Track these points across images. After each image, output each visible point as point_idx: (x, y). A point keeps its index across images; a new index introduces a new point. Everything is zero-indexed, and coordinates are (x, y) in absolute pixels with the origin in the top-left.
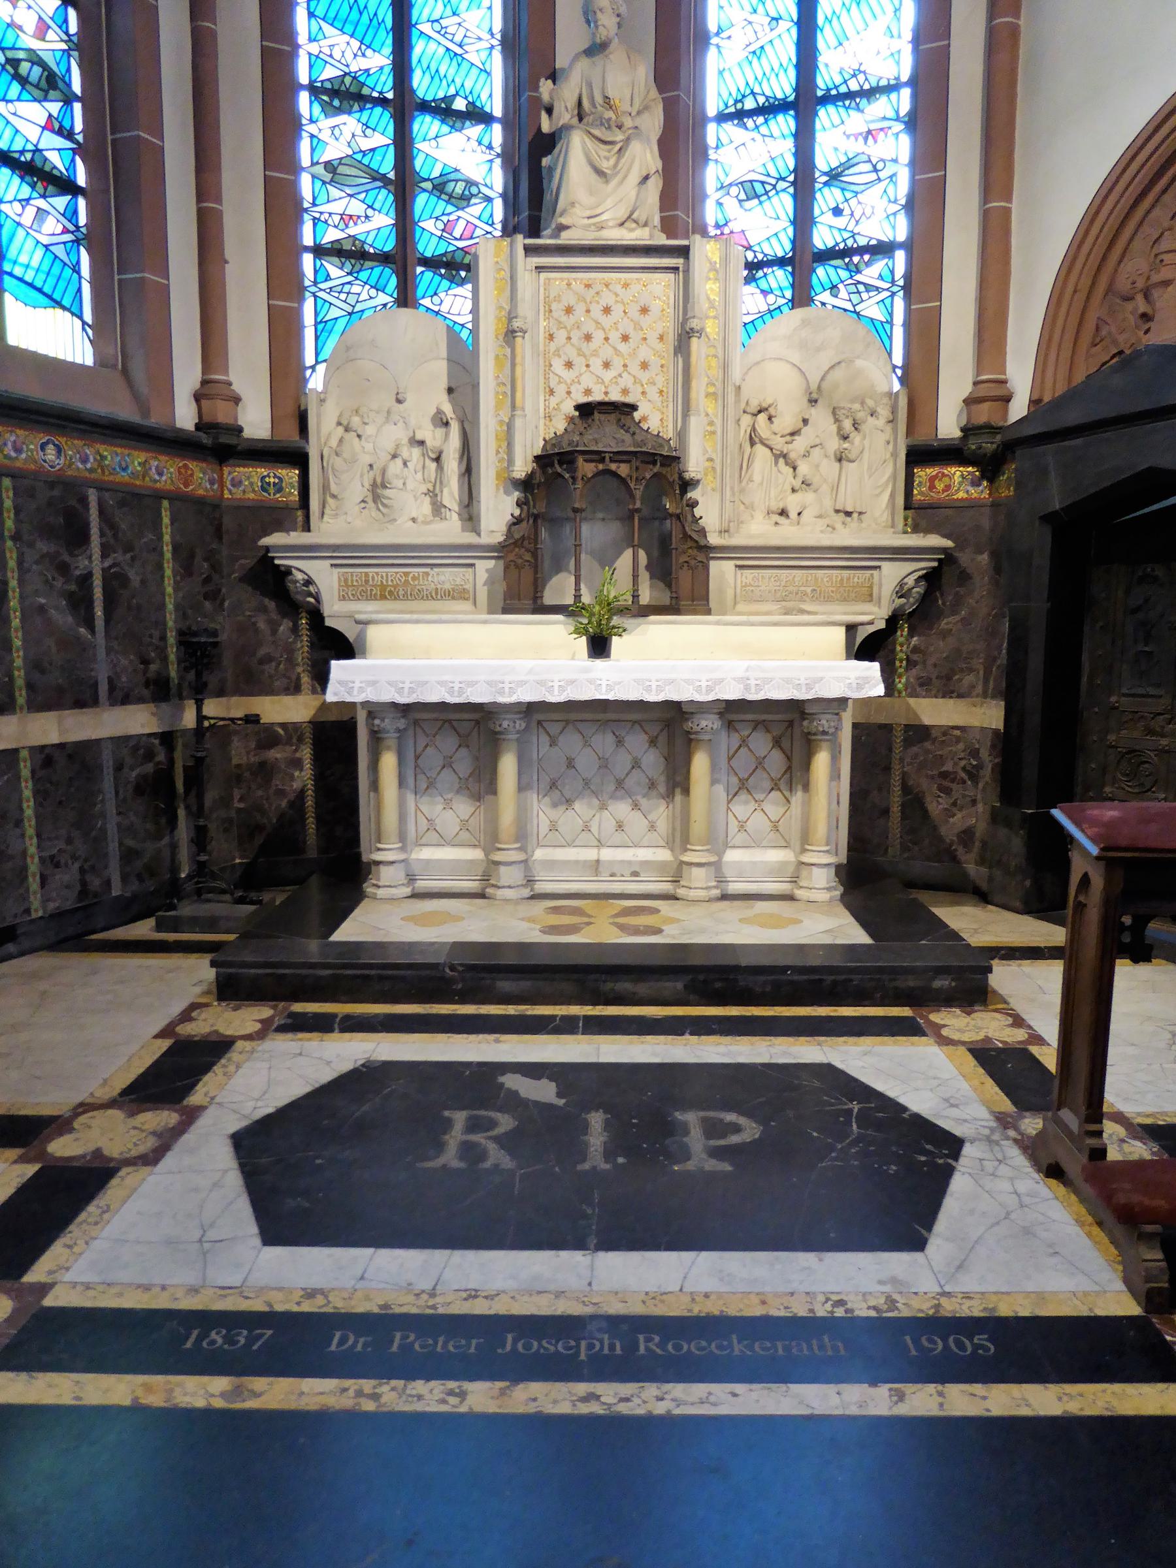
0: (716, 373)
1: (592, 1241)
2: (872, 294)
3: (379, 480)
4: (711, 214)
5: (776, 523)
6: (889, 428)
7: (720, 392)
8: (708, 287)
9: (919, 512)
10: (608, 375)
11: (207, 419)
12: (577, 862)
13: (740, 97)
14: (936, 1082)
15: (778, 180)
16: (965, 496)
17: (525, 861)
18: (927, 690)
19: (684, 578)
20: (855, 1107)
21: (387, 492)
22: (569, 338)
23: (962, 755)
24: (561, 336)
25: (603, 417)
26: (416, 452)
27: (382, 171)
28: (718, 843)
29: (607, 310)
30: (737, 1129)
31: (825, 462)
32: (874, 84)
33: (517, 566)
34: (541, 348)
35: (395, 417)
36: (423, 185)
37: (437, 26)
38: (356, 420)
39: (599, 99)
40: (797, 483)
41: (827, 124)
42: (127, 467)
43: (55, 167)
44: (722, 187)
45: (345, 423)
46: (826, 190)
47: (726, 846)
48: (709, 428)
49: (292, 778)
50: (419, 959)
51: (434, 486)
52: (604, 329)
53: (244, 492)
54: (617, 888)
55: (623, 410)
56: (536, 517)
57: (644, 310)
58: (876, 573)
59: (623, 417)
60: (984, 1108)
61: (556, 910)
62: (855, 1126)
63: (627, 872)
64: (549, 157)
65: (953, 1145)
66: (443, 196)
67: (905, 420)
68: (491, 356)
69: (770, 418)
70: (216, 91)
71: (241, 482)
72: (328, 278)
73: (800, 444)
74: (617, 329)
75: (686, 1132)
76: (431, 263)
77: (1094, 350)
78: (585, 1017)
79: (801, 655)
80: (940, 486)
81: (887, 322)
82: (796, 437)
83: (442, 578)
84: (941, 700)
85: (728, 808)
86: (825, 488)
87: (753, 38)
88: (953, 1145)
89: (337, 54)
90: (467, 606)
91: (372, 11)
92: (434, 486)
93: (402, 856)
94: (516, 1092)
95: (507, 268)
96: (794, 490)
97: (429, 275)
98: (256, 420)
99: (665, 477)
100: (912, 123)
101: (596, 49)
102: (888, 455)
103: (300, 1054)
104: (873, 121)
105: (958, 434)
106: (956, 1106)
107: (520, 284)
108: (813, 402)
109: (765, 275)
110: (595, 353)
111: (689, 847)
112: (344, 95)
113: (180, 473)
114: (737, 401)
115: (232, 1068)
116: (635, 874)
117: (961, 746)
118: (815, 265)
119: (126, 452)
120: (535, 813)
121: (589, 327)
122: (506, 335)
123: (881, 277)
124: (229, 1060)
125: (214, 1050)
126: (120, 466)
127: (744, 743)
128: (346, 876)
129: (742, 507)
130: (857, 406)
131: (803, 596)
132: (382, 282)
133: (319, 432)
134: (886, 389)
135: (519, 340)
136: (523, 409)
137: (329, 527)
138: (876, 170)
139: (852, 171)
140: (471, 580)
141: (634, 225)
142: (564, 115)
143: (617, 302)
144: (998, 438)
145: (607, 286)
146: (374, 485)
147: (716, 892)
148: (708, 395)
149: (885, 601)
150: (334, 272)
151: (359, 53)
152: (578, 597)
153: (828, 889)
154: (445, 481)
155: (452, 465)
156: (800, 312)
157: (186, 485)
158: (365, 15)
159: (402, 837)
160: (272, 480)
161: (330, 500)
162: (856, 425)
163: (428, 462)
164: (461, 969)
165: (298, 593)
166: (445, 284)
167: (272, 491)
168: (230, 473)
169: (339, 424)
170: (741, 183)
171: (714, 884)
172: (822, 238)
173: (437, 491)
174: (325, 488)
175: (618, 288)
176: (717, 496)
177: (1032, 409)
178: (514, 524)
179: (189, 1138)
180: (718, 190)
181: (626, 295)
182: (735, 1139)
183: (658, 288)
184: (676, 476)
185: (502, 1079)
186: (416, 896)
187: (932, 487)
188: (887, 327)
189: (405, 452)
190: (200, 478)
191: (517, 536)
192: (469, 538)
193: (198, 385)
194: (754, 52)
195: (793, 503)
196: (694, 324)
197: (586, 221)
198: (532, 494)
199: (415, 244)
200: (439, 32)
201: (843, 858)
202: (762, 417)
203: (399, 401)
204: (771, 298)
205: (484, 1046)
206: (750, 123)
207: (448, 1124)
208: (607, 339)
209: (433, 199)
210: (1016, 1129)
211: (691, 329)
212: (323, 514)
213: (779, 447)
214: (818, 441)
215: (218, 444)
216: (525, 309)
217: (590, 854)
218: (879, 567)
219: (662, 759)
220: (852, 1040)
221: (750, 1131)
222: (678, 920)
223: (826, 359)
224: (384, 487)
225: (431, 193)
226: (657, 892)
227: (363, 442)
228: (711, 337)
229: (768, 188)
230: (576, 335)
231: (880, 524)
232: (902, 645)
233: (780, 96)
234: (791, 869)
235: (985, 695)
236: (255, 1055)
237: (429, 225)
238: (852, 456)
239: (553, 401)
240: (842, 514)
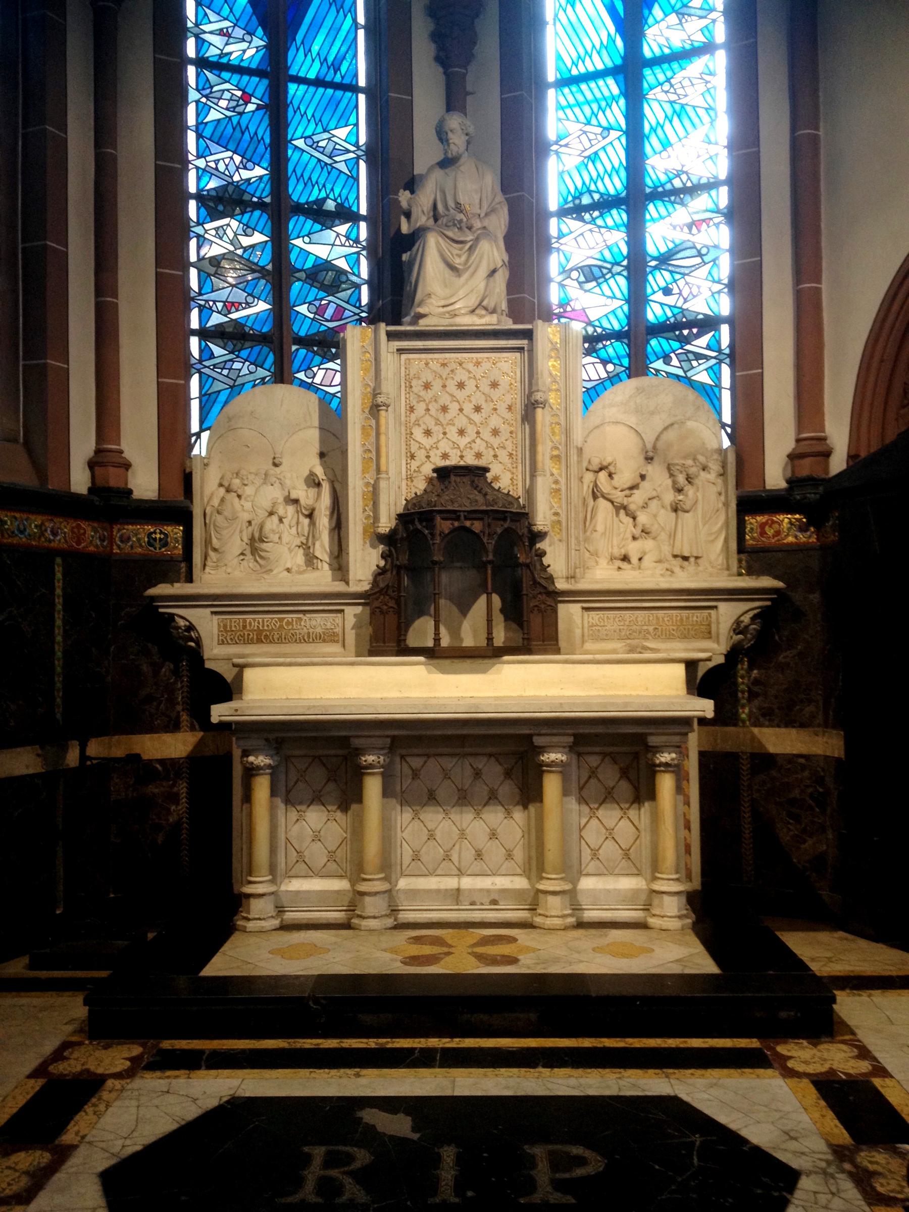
0: (559, 438)
1: (789, 1196)
2: (701, 362)
3: (257, 535)
4: (554, 295)
5: (619, 568)
6: (720, 481)
7: (563, 456)
8: (550, 364)
9: (751, 556)
10: (463, 442)
11: (100, 483)
12: (438, 891)
13: (577, 194)
14: (777, 1115)
15: (613, 264)
16: (794, 540)
17: (389, 891)
18: (770, 720)
19: (535, 621)
20: (698, 1139)
21: (264, 546)
22: (428, 410)
23: (808, 782)
24: (420, 408)
25: (458, 479)
26: (291, 509)
27: (261, 264)
28: (572, 871)
29: (461, 385)
30: (581, 1161)
31: (662, 511)
32: (695, 181)
33: (382, 612)
34: (403, 418)
35: (273, 479)
36: (297, 275)
37: (309, 142)
38: (236, 482)
39: (451, 204)
40: (637, 532)
41: (655, 215)
42: (25, 529)
44: (564, 271)
45: (226, 484)
46: (657, 273)
47: (580, 873)
48: (554, 486)
49: (169, 812)
50: (284, 993)
51: (307, 539)
52: (458, 402)
53: (132, 547)
54: (477, 916)
55: (475, 474)
56: (399, 568)
57: (494, 385)
58: (713, 612)
59: (476, 479)
60: (823, 1141)
61: (417, 940)
62: (696, 1160)
63: (486, 900)
64: (409, 253)
65: (789, 1177)
66: (315, 284)
67: (734, 473)
68: (358, 427)
69: (610, 475)
70: (115, 225)
71: (129, 539)
72: (212, 356)
73: (638, 497)
74: (470, 401)
75: (534, 1166)
76: (302, 342)
77: (902, 412)
78: (442, 1049)
79: (651, 685)
80: (770, 532)
81: (716, 386)
82: (635, 491)
83: (314, 623)
84: (783, 730)
85: (581, 837)
86: (663, 536)
87: (587, 145)
88: (789, 1177)
89: (221, 167)
90: (335, 648)
91: (252, 130)
92: (307, 539)
93: (272, 889)
94: (374, 1126)
95: (371, 350)
96: (634, 538)
97: (303, 352)
98: (144, 483)
99: (515, 531)
100: (731, 215)
101: (447, 163)
102: (721, 505)
103: (168, 1092)
104: (697, 213)
105: (783, 485)
106: (796, 1139)
107: (383, 366)
108: (649, 459)
109: (605, 346)
110: (451, 423)
111: (544, 875)
112: (226, 201)
113: (73, 532)
114: (579, 462)
115: (102, 1107)
116: (494, 902)
117: (806, 773)
118: (649, 337)
119: (25, 516)
120: (399, 843)
121: (445, 399)
122: (371, 408)
123: (708, 347)
124: (100, 1099)
125: (87, 1088)
126: (19, 529)
127: (593, 773)
128: (220, 910)
129: (587, 554)
130: (690, 462)
131: (646, 635)
132: (261, 358)
133: (202, 493)
134: (716, 446)
135: (383, 413)
136: (387, 473)
137: (211, 579)
138: (700, 255)
139: (679, 256)
140: (341, 625)
141: (484, 312)
142: (422, 219)
143: (470, 378)
144: (821, 489)
145: (460, 365)
146: (252, 539)
147: (571, 920)
148: (552, 457)
149: (723, 639)
150: (217, 351)
151: (241, 166)
152: (437, 640)
153: (680, 917)
154: (317, 535)
155: (324, 521)
156: (635, 382)
157: (79, 543)
158: (247, 134)
159: (272, 869)
160: (158, 536)
161: (211, 553)
162: (689, 479)
163: (302, 518)
164: (323, 1002)
165: (180, 638)
166: (318, 359)
167: (158, 546)
168: (119, 530)
169: (221, 485)
170: (581, 268)
171: (570, 912)
172: (654, 313)
173: (310, 544)
174: (208, 542)
175: (470, 366)
176: (563, 546)
177: (851, 463)
178: (379, 574)
179: (59, 1177)
180: (560, 274)
181: (479, 372)
182: (580, 1172)
183: (506, 366)
184: (525, 531)
185: (360, 1114)
186: (286, 927)
187: (763, 533)
188: (716, 390)
189: (281, 511)
190: (90, 537)
191: (382, 585)
192: (339, 587)
193: (92, 454)
194: (589, 157)
195: (634, 549)
196: (538, 396)
197: (441, 310)
198: (395, 549)
199: (290, 327)
200: (311, 146)
201: (696, 884)
202: (603, 475)
203: (276, 465)
204: (610, 367)
205: (344, 1081)
206: (587, 217)
207: (307, 1159)
208: (461, 410)
209: (307, 286)
210: (853, 1162)
211: (536, 401)
212: (205, 565)
213: (619, 500)
214: (654, 494)
215: (110, 502)
216: (389, 387)
217: (451, 883)
218: (716, 607)
219: (517, 790)
220: (699, 1072)
221: (594, 1164)
222: (535, 950)
223: (658, 422)
224: (262, 541)
225: (305, 282)
226: (514, 920)
227: (243, 502)
228: (554, 407)
229: (605, 271)
230: (433, 408)
231: (716, 567)
232: (742, 677)
233: (612, 192)
234: (643, 897)
235: (826, 725)
236: (125, 1094)
237: (303, 309)
238: (687, 507)
239: (414, 465)
240: (679, 559)
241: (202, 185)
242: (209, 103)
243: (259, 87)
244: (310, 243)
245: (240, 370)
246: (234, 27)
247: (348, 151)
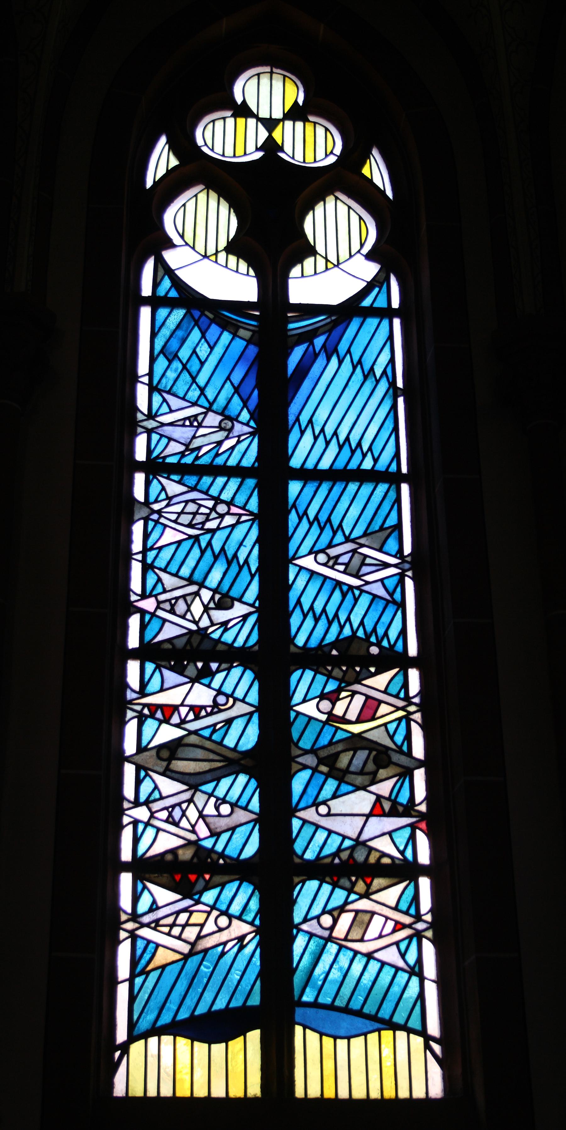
37: (322, 558)
43: (384, 855)
151: (212, 605)
200: (325, 565)
241: (148, 635)
242: (162, 520)
243: (248, 496)
244: (329, 814)
245: (202, 926)
246: (206, 414)
247: (386, 565)
